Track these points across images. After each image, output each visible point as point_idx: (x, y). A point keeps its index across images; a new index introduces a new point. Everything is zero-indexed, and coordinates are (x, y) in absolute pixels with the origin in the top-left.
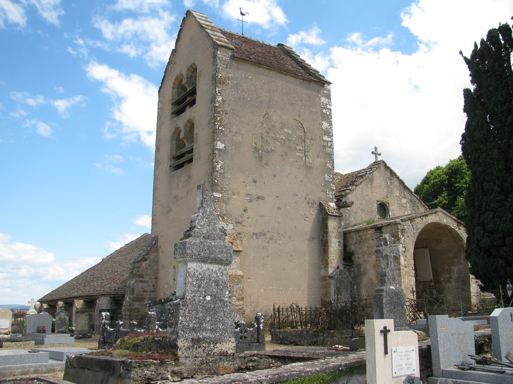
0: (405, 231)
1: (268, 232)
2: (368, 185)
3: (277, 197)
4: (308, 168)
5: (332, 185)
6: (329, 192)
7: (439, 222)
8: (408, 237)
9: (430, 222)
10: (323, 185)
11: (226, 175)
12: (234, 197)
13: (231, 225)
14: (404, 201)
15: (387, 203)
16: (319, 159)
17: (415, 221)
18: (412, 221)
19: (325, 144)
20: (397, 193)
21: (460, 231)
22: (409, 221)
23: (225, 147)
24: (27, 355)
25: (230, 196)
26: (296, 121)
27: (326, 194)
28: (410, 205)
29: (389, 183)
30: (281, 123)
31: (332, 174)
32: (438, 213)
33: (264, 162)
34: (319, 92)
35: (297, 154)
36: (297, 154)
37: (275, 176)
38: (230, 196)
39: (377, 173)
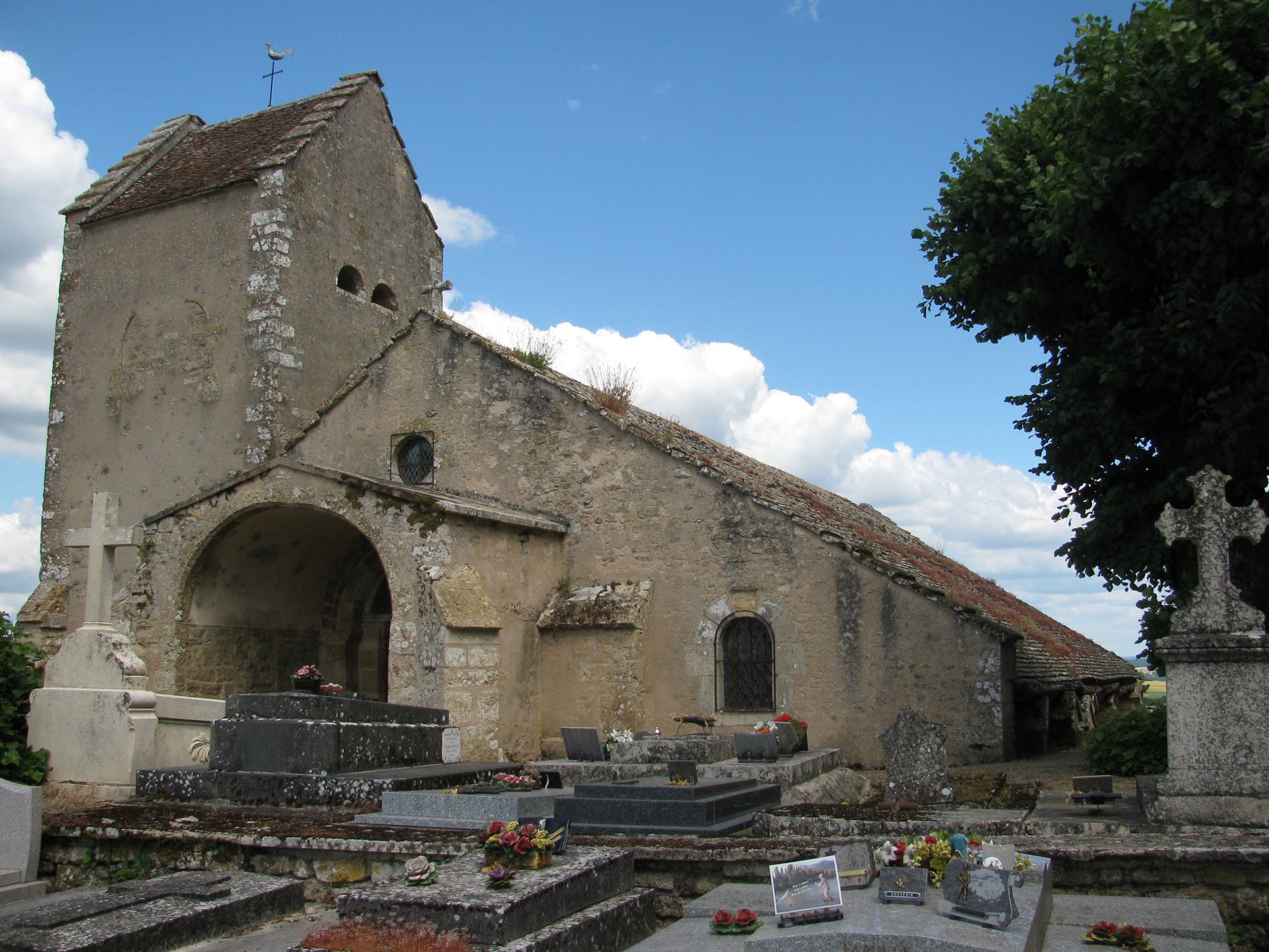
0: (157, 549)
1: (125, 571)
2: (366, 398)
3: (143, 492)
4: (207, 404)
5: (260, 430)
6: (252, 449)
7: (275, 500)
8: (164, 563)
9: (239, 507)
10: (238, 436)
11: (63, 472)
12: (72, 512)
13: (67, 569)
14: (499, 408)
15: (427, 432)
16: (234, 375)
17: (190, 515)
18: (180, 517)
19: (251, 331)
20: (470, 391)
21: (357, 513)
22: (171, 520)
23: (63, 418)
24: (945, 887)
25: (66, 512)
26: (188, 304)
27: (246, 457)
28: (524, 415)
29: (440, 372)
30: (161, 322)
31: (262, 402)
32: (273, 473)
33: (123, 423)
34: (245, 202)
35: (187, 381)
36: (187, 381)
37: (140, 447)
38: (66, 512)
39: (404, 353)
